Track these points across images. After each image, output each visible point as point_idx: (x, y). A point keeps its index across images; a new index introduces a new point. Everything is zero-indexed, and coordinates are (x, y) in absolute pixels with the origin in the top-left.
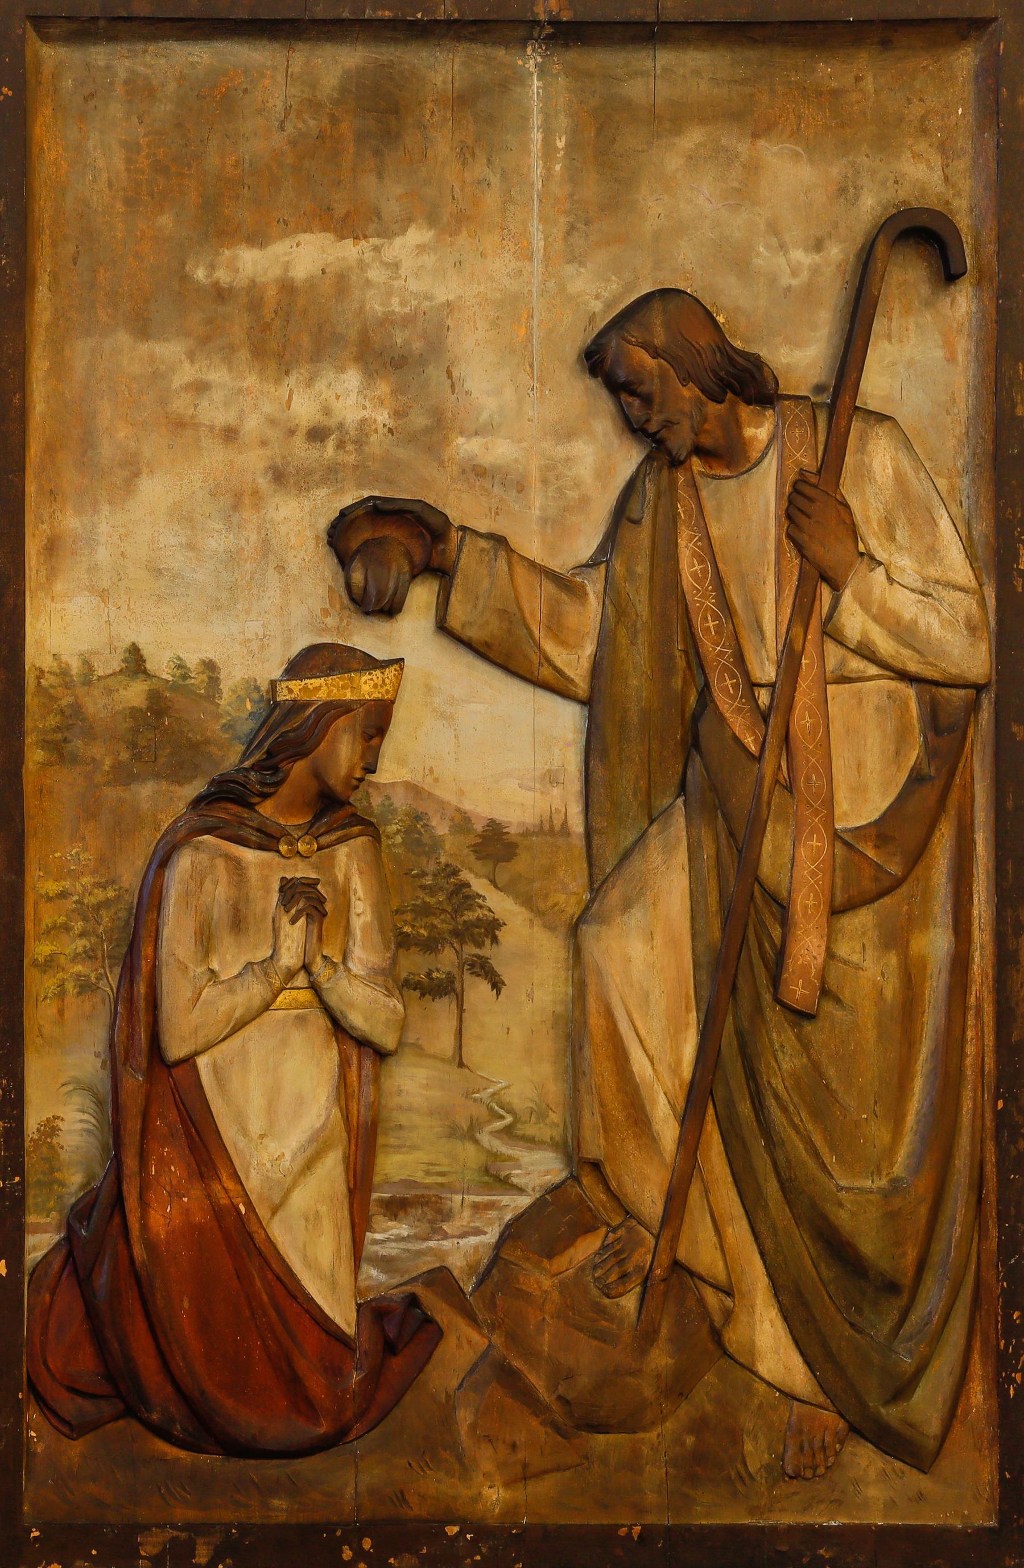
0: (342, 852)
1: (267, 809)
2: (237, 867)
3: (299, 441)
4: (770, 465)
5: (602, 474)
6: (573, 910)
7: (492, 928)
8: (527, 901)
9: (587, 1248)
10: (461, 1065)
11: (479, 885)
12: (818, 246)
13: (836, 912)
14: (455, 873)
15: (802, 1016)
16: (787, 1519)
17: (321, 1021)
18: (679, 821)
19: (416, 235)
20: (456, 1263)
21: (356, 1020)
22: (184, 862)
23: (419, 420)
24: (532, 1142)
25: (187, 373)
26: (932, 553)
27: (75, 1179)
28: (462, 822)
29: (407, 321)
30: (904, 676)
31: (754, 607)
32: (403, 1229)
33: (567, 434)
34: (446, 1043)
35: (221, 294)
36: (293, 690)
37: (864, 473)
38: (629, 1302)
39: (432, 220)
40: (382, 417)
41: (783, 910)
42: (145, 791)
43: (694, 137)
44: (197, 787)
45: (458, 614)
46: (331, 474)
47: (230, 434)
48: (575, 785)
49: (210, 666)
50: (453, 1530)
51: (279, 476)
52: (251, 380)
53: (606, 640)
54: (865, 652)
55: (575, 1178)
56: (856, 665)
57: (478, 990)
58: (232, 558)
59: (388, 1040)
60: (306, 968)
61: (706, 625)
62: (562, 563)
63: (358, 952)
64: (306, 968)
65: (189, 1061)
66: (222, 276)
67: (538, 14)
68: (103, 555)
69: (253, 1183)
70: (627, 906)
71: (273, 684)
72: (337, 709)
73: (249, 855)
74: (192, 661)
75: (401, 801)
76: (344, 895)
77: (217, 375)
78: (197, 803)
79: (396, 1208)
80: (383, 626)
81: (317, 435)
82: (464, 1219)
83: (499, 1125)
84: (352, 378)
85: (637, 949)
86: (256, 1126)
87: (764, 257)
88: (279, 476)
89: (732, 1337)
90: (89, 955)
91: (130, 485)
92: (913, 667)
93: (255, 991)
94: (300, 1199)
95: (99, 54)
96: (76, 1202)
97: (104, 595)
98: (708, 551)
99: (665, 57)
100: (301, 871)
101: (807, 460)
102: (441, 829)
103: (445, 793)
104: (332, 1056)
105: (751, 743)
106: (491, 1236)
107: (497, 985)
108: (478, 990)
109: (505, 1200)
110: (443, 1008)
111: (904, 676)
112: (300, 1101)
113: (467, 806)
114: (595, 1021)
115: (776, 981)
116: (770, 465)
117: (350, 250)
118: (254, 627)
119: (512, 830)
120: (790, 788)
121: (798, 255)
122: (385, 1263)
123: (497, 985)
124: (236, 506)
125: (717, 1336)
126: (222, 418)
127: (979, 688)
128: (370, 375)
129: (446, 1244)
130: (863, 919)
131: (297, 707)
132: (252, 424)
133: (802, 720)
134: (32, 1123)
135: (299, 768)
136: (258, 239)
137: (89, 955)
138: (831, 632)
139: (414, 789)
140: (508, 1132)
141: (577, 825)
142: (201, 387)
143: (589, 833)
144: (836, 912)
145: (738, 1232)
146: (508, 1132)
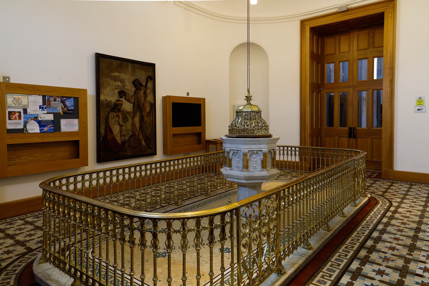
0: (120, 113)
1: (115, 110)
2: (114, 114)
3: (116, 86)
4: (143, 90)
5: (134, 90)
6: (132, 117)
7: (128, 118)
8: (130, 116)
9: (134, 138)
11: (127, 115)
12: (144, 77)
13: (147, 117)
15: (145, 123)
16: (145, 153)
17: (118, 124)
18: (138, 111)
19: (123, 74)
20: (126, 139)
21: (121, 124)
22: (110, 114)
23: (123, 85)
24: (130, 131)
25: (109, 81)
26: (151, 96)
27: (103, 135)
28: (126, 111)
29: (123, 79)
30: (150, 103)
31: (142, 98)
32: (123, 137)
33: (132, 87)
34: (125, 125)
35: (112, 76)
36: (117, 102)
37: (148, 91)
38: (136, 141)
39: (124, 73)
40: (121, 85)
41: (144, 117)
42: (107, 109)
43: (138, 70)
44: (110, 109)
45: (126, 98)
46: (118, 89)
47: (112, 85)
48: (132, 109)
49: (111, 101)
51: (115, 88)
52: (113, 82)
53: (134, 100)
54: (148, 102)
55: (133, 134)
56: (147, 102)
57: (127, 122)
58: (112, 93)
59: (123, 125)
60: (118, 121)
61: (140, 99)
62: (131, 95)
63: (121, 120)
64: (118, 121)
65: (111, 127)
66: (112, 75)
67: (135, 239)
68: (104, 93)
69: (115, 135)
70: (136, 116)
71: (172, 251)
72: (119, 104)
73: (114, 113)
74: (110, 100)
75: (123, 110)
76: (120, 116)
77: (111, 81)
78: (111, 110)
79: (123, 136)
80: (121, 99)
81: (117, 86)
82: (127, 136)
84: (119, 82)
85: (136, 119)
86: (115, 131)
87: (142, 77)
88: (115, 88)
89: (142, 143)
90: (104, 120)
91: (106, 88)
92: (150, 103)
93: (115, 122)
95: (104, 59)
96: (338, 233)
97: (104, 95)
98: (140, 95)
99: (137, 65)
100: (117, 114)
101: (145, 90)
102: (125, 112)
103: (125, 109)
104: (119, 126)
105: (142, 107)
106: (128, 137)
108: (127, 122)
110: (125, 123)
111: (150, 103)
114: (134, 124)
115: (144, 121)
116: (143, 90)
117: (119, 74)
118: (114, 98)
120: (144, 109)
121: (144, 78)
122: (122, 140)
124: (113, 90)
125: (141, 143)
126: (112, 84)
127: (153, 104)
128: (120, 82)
130: (148, 117)
131: (117, 104)
132: (114, 85)
133: (145, 105)
134: (101, 131)
135: (117, 108)
136: (114, 73)
137: (104, 120)
138: (146, 100)
139: (123, 109)
140: (129, 131)
141: (133, 112)
142: (110, 82)
143: (133, 112)
144: (147, 117)
145: (142, 136)
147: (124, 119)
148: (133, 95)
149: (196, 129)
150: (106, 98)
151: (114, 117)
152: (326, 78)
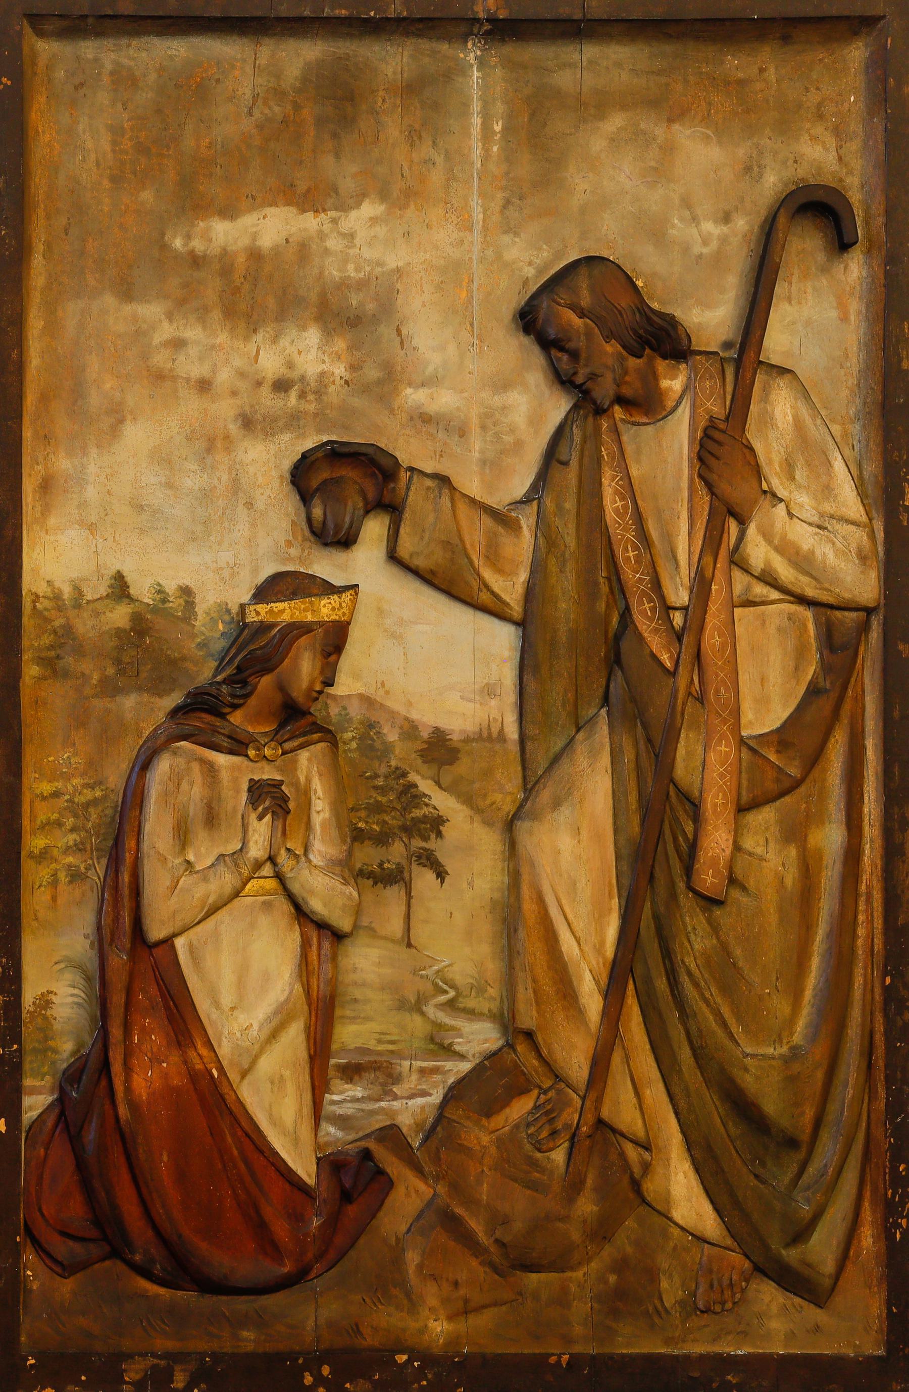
0: (304, 756)
1: (237, 718)
2: (210, 770)
3: (265, 391)
4: (684, 413)
5: (535, 421)
6: (509, 807)
7: (436, 824)
8: (468, 800)
9: (521, 1108)
10: (409, 945)
11: (425, 786)
12: (726, 218)
13: (742, 809)
14: (404, 775)
15: (712, 902)
16: (699, 1349)
17: (285, 907)
18: (603, 729)
19: (369, 209)
20: (405, 1121)
21: (316, 905)
22: (163, 765)
23: (372, 373)
24: (472, 1014)
25: (166, 331)
26: (827, 491)
27: (66, 1047)
28: (410, 730)
29: (362, 285)
30: (802, 600)
31: (669, 539)
32: (358, 1091)
33: (503, 385)
34: (396, 926)
35: (196, 261)
36: (260, 613)
37: (767, 420)
38: (559, 1156)
39: (384, 195)
40: (339, 370)
41: (695, 808)
42: (129, 702)
44: (175, 699)
45: (407, 545)
46: (294, 421)
47: (204, 386)
48: (511, 697)
49: (186, 591)
50: (402, 1358)
51: (247, 423)
52: (223, 338)
53: (538, 568)
54: (768, 579)
55: (510, 1046)
56: (760, 590)
57: (424, 879)
58: (206, 495)
59: (344, 924)
61: (627, 555)
62: (499, 500)
63: (318, 845)
64: (272, 859)
65: (168, 942)
66: (197, 245)
68: (91, 493)
69: (225, 1050)
70: (556, 804)
72: (299, 629)
73: (221, 759)
74: (171, 587)
75: (356, 711)
76: (306, 795)
77: (193, 333)
78: (175, 713)
79: (351, 1072)
80: (340, 556)
81: (281, 386)
82: (411, 1082)
83: (443, 998)
84: (313, 336)
85: (565, 843)
86: (227, 1000)
87: (678, 228)
88: (247, 423)
89: (650, 1187)
90: (79, 848)
91: (115, 430)
92: (810, 592)
93: (226, 880)
94: (267, 1064)
95: (88, 48)
97: (92, 528)
98: (629, 489)
99: (591, 51)
100: (268, 773)
101: (716, 408)
102: (392, 736)
103: (395, 704)
104: (294, 938)
105: (667, 660)
106: (436, 1097)
107: (441, 874)
108: (424, 879)
109: (448, 1065)
110: (394, 895)
111: (802, 600)
112: (266, 977)
113: (414, 715)
114: (529, 907)
115: (688, 870)
116: (684, 413)
117: (310, 222)
118: (226, 557)
119: (455, 737)
120: (701, 699)
121: (709, 226)
122: (342, 1121)
123: (441, 874)
124: (210, 449)
125: (636, 1186)
126: (197, 371)
127: (869, 611)
128: (328, 333)
129: (396, 1104)
130: (766, 816)
131: (264, 628)
132: (224, 376)
133: (712, 639)
134: (29, 997)
135: (265, 682)
136: (229, 212)
137: (79, 848)
138: (738, 561)
139: (367, 701)
140: (451, 1005)
141: (512, 732)
142: (178, 344)
143: (522, 740)
144: (742, 809)
145: (656, 1094)
146: (451, 1005)
147: (382, 839)
148: (526, 501)
149: (310, 719)
150: (114, 564)
151: (211, 819)
152: (808, 994)
